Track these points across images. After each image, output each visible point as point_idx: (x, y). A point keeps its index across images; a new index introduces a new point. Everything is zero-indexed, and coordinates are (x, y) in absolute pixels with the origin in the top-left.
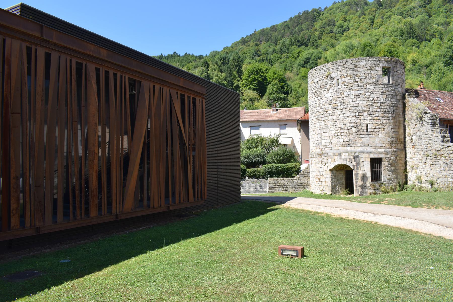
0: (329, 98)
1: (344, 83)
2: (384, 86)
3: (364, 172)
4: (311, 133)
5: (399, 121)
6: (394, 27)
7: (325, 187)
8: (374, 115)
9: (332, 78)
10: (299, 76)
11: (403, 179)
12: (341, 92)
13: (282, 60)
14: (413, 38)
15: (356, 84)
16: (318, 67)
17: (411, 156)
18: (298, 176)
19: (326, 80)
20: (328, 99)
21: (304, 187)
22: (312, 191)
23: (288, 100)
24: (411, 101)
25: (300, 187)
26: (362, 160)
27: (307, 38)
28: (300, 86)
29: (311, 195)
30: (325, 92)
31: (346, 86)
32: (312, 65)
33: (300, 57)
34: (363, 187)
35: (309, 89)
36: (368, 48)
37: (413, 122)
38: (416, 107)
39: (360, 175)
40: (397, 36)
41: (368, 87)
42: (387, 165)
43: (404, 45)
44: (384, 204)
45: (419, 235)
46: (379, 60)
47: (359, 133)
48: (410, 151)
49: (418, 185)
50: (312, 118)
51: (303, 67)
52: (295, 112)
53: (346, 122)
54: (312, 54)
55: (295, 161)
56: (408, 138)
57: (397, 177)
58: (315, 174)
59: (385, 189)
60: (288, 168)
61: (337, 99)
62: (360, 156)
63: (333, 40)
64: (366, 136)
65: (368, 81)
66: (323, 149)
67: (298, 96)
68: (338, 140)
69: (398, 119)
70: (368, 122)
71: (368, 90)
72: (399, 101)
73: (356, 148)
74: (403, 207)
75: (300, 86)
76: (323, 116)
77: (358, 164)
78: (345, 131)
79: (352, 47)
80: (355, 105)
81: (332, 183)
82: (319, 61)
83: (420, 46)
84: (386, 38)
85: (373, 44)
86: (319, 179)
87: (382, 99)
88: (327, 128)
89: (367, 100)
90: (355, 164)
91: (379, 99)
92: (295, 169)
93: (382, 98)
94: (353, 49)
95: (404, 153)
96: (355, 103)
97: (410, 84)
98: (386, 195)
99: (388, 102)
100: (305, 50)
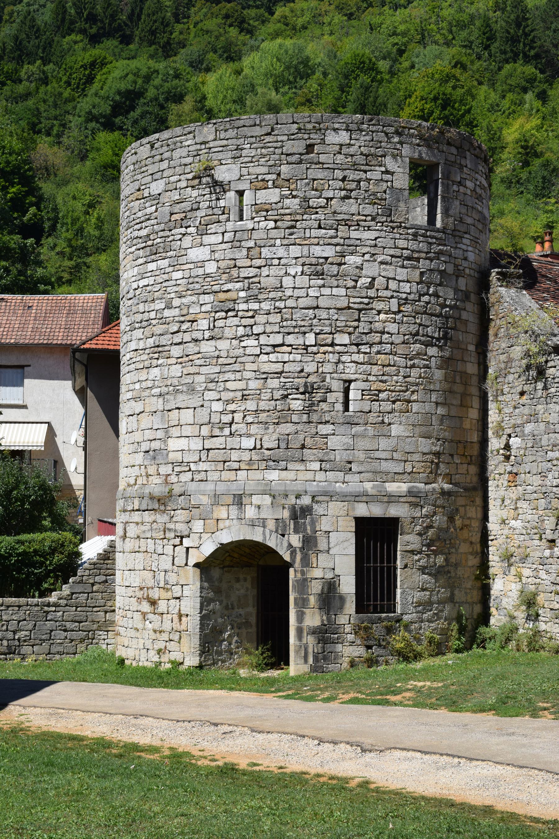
0: (201, 264)
1: (262, 209)
2: (415, 235)
3: (329, 575)
4: (125, 409)
5: (464, 373)
6: (461, 10)
7: (176, 637)
8: (375, 349)
9: (219, 188)
10: (88, 163)
11: (472, 604)
12: (251, 244)
13: (21, 88)
14: (527, 59)
15: (311, 220)
16: (165, 135)
17: (504, 514)
18: (66, 590)
19: (195, 193)
20: (200, 271)
21: (89, 638)
22: (121, 652)
23: (39, 263)
24: (510, 302)
25: (74, 635)
26: (324, 525)
27: (128, 9)
28: (91, 205)
29: (119, 672)
30: (188, 239)
31: (272, 224)
32: (143, 123)
33: (96, 85)
34: (326, 635)
35: (123, 223)
36: (365, 79)
37: (514, 382)
38: (525, 324)
39: (316, 588)
40: (468, 45)
41: (354, 235)
42: (416, 546)
43: (492, 84)
44: (401, 704)
45: (514, 826)
46: (397, 133)
47: (315, 417)
48: (502, 492)
49: (525, 628)
50: (133, 346)
51: (109, 125)
52: (62, 316)
53: (266, 368)
54: (148, 78)
55: (59, 523)
56: (495, 444)
57: (452, 594)
58: (135, 580)
59: (409, 645)
60: (25, 553)
61: (235, 272)
62: (318, 509)
63: (233, 32)
64: (342, 429)
65: (354, 209)
66: (173, 479)
67: (83, 247)
68: (233, 442)
69: (460, 366)
70: (350, 371)
71: (351, 247)
72: (466, 296)
73: (302, 476)
74: (467, 717)
75: (91, 205)
76: (177, 338)
77: (309, 543)
78: (263, 405)
79: (298, 71)
80: (303, 302)
81: (202, 618)
82: (174, 107)
83: (550, 93)
84: (432, 49)
85: (384, 65)
86: (153, 603)
87: (406, 287)
88: (191, 389)
89: (351, 284)
90: (296, 540)
91: (393, 285)
92: (57, 558)
93: (404, 280)
94: (308, 76)
95: (479, 501)
96: (302, 293)
97: (512, 236)
98: (410, 666)
99: (426, 298)
100: (117, 57)
